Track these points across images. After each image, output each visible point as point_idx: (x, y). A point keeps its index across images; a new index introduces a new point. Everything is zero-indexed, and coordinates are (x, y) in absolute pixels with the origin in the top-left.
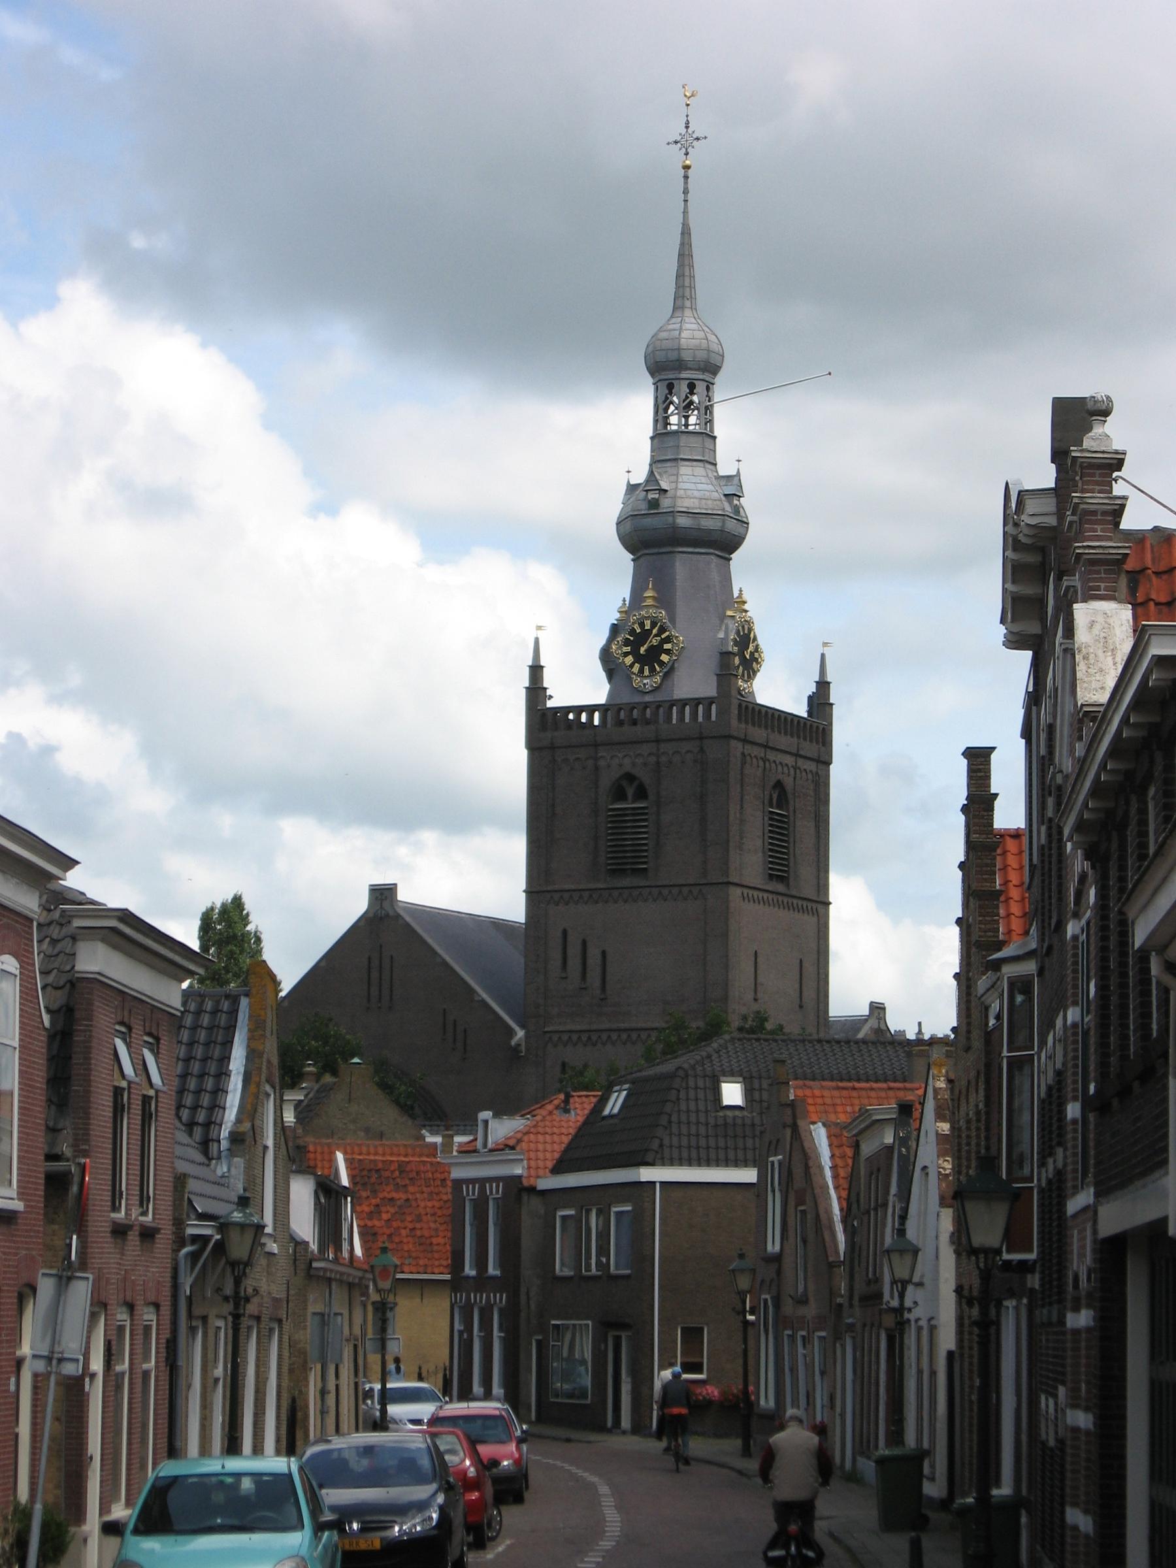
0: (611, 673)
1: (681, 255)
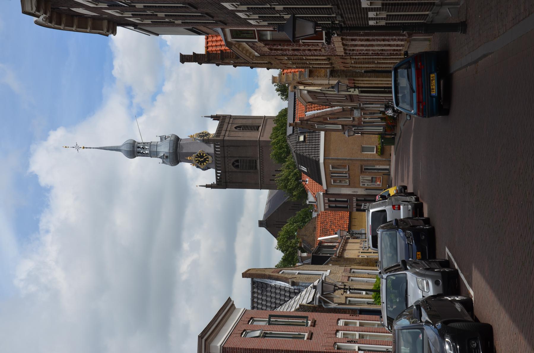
0: (209, 168)
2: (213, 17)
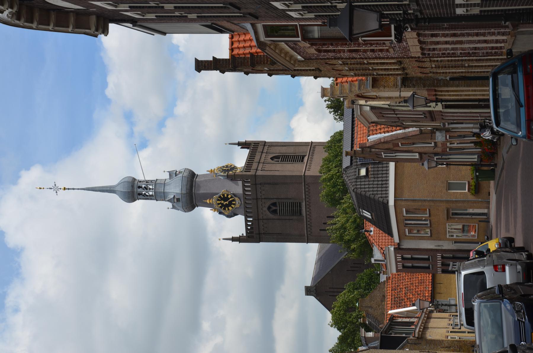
0: (236, 214)
1: (88, 190)
2: (239, 9)
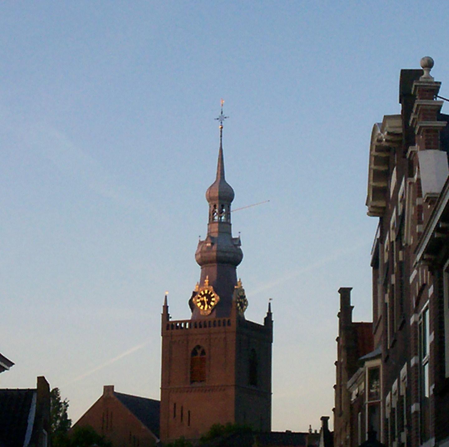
2: (401, 328)
